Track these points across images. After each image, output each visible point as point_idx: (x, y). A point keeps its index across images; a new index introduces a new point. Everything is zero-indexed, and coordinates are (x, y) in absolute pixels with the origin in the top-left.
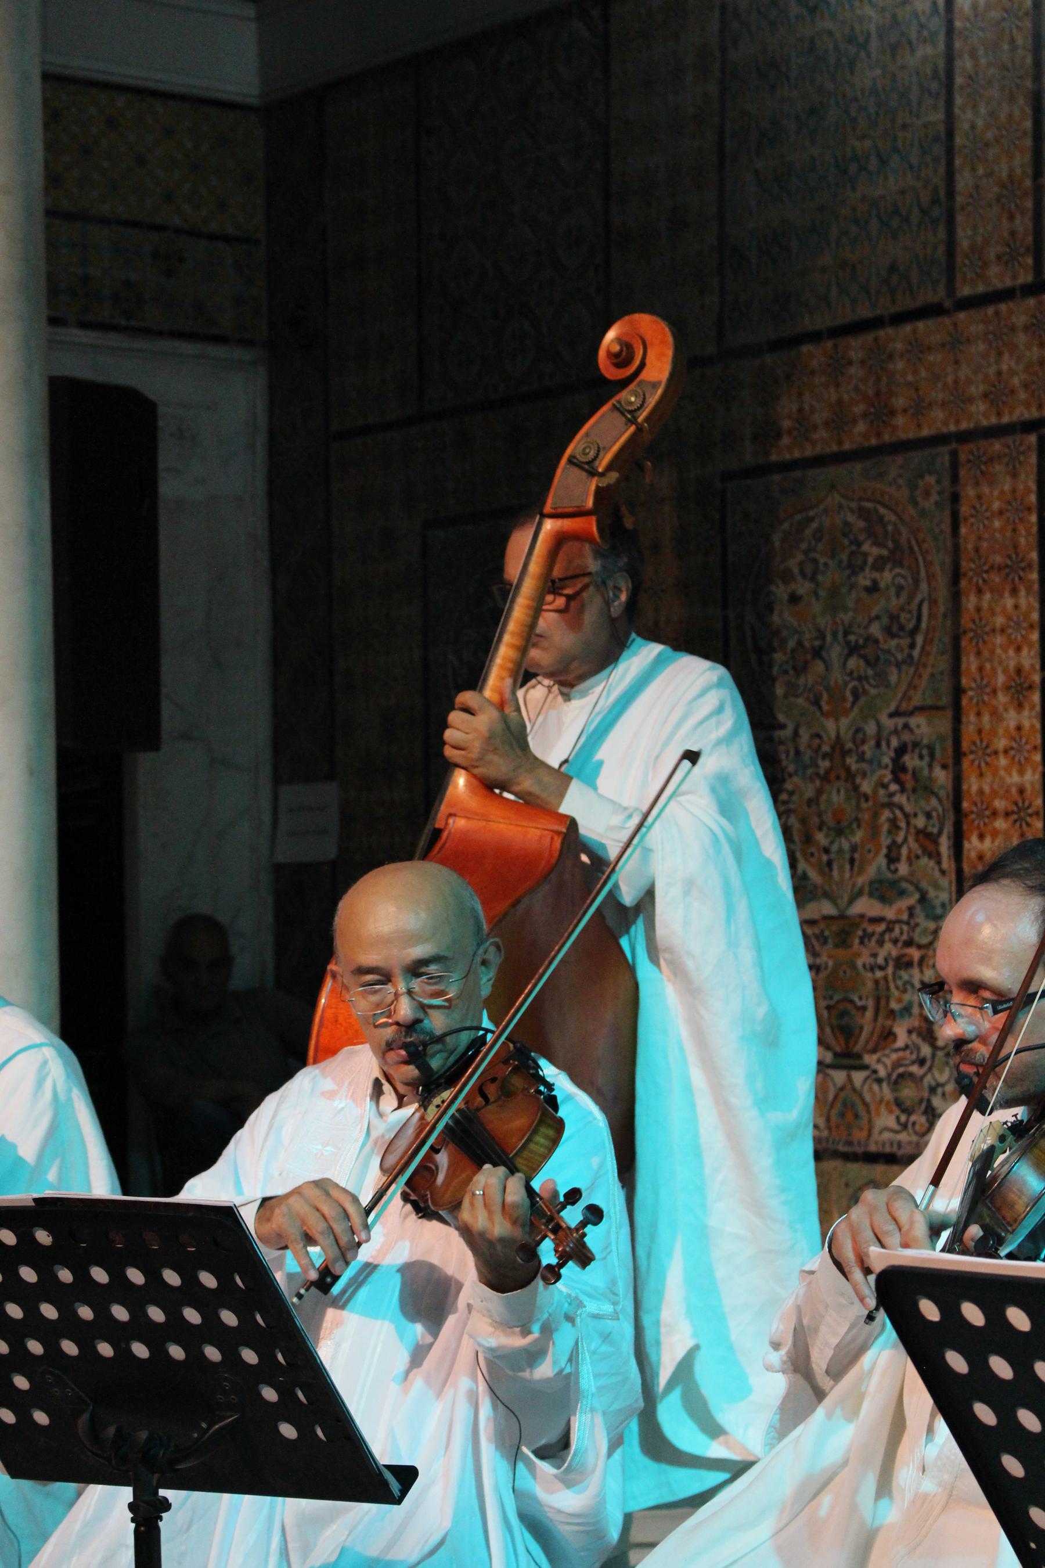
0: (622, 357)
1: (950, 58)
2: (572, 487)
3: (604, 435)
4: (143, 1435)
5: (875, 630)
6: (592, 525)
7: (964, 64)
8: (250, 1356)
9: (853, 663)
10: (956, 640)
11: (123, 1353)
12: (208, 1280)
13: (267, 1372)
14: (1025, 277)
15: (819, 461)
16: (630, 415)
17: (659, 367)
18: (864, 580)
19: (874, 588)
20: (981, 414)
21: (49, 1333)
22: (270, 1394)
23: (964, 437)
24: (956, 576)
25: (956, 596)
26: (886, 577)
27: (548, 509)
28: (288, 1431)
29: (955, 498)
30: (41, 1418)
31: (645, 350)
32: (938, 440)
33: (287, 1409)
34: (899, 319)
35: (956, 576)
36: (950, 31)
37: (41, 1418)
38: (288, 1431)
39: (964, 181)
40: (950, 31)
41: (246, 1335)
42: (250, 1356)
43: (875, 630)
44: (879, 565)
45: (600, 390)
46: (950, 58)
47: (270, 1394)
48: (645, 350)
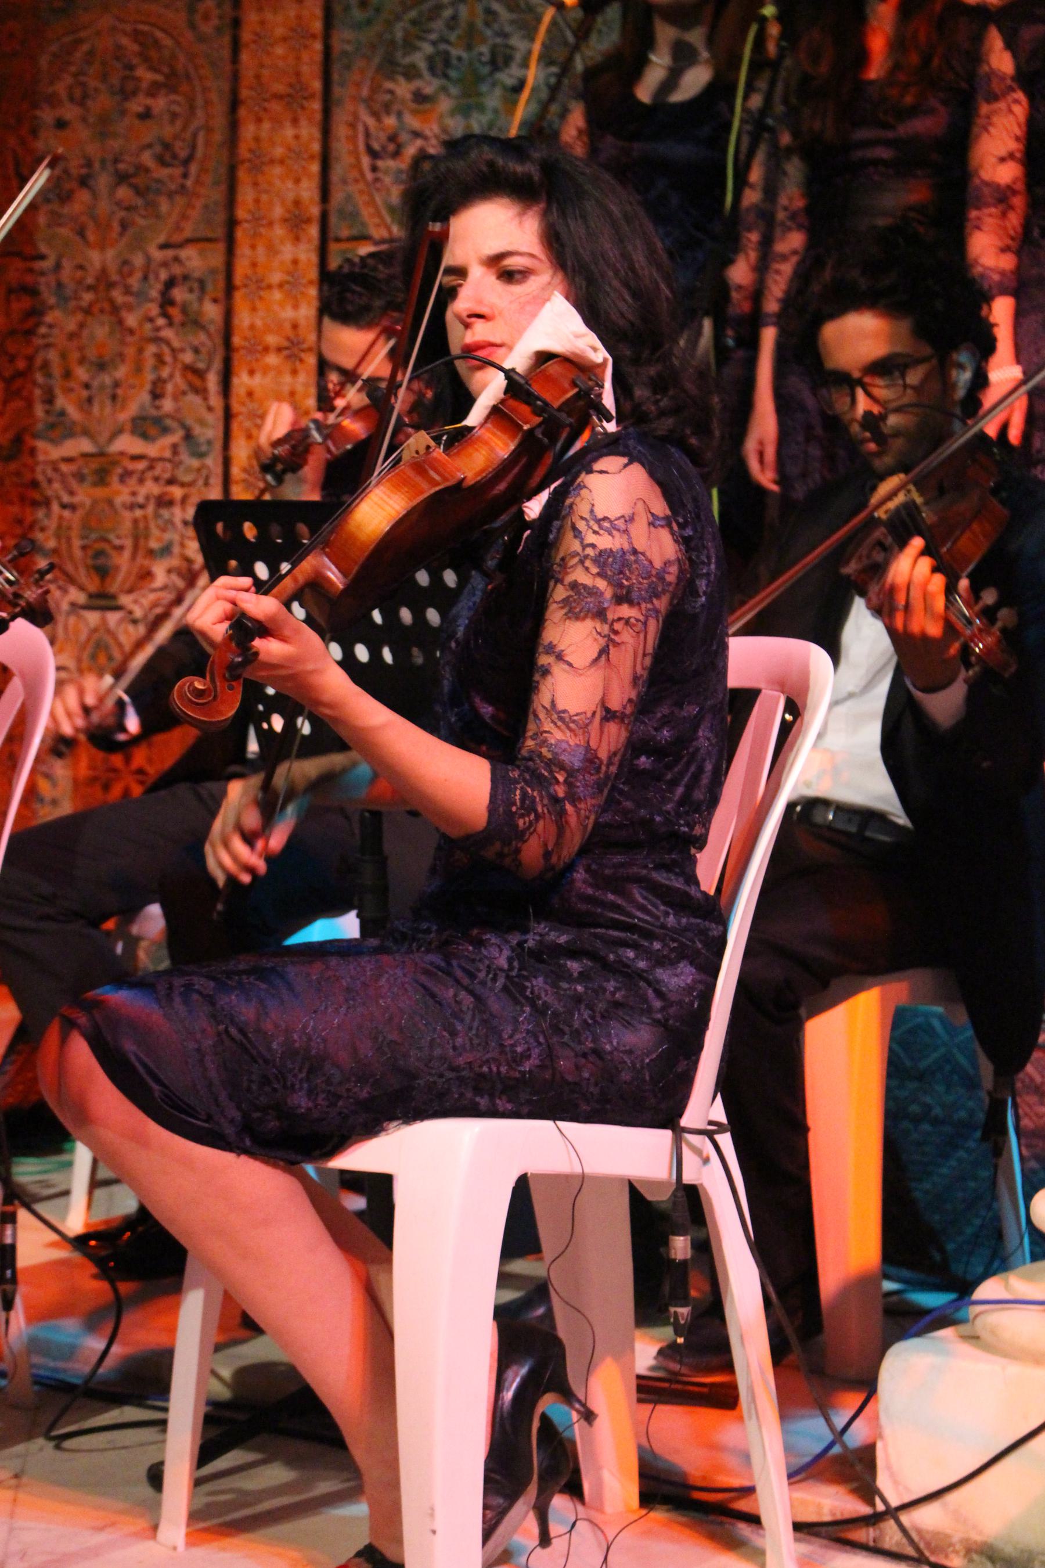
5: (147, 158)
9: (123, 192)
18: (136, 106)
19: (146, 115)
24: (234, 104)
25: (234, 126)
26: (160, 104)
29: (236, 23)
35: (234, 104)
43: (147, 158)
44: (154, 90)
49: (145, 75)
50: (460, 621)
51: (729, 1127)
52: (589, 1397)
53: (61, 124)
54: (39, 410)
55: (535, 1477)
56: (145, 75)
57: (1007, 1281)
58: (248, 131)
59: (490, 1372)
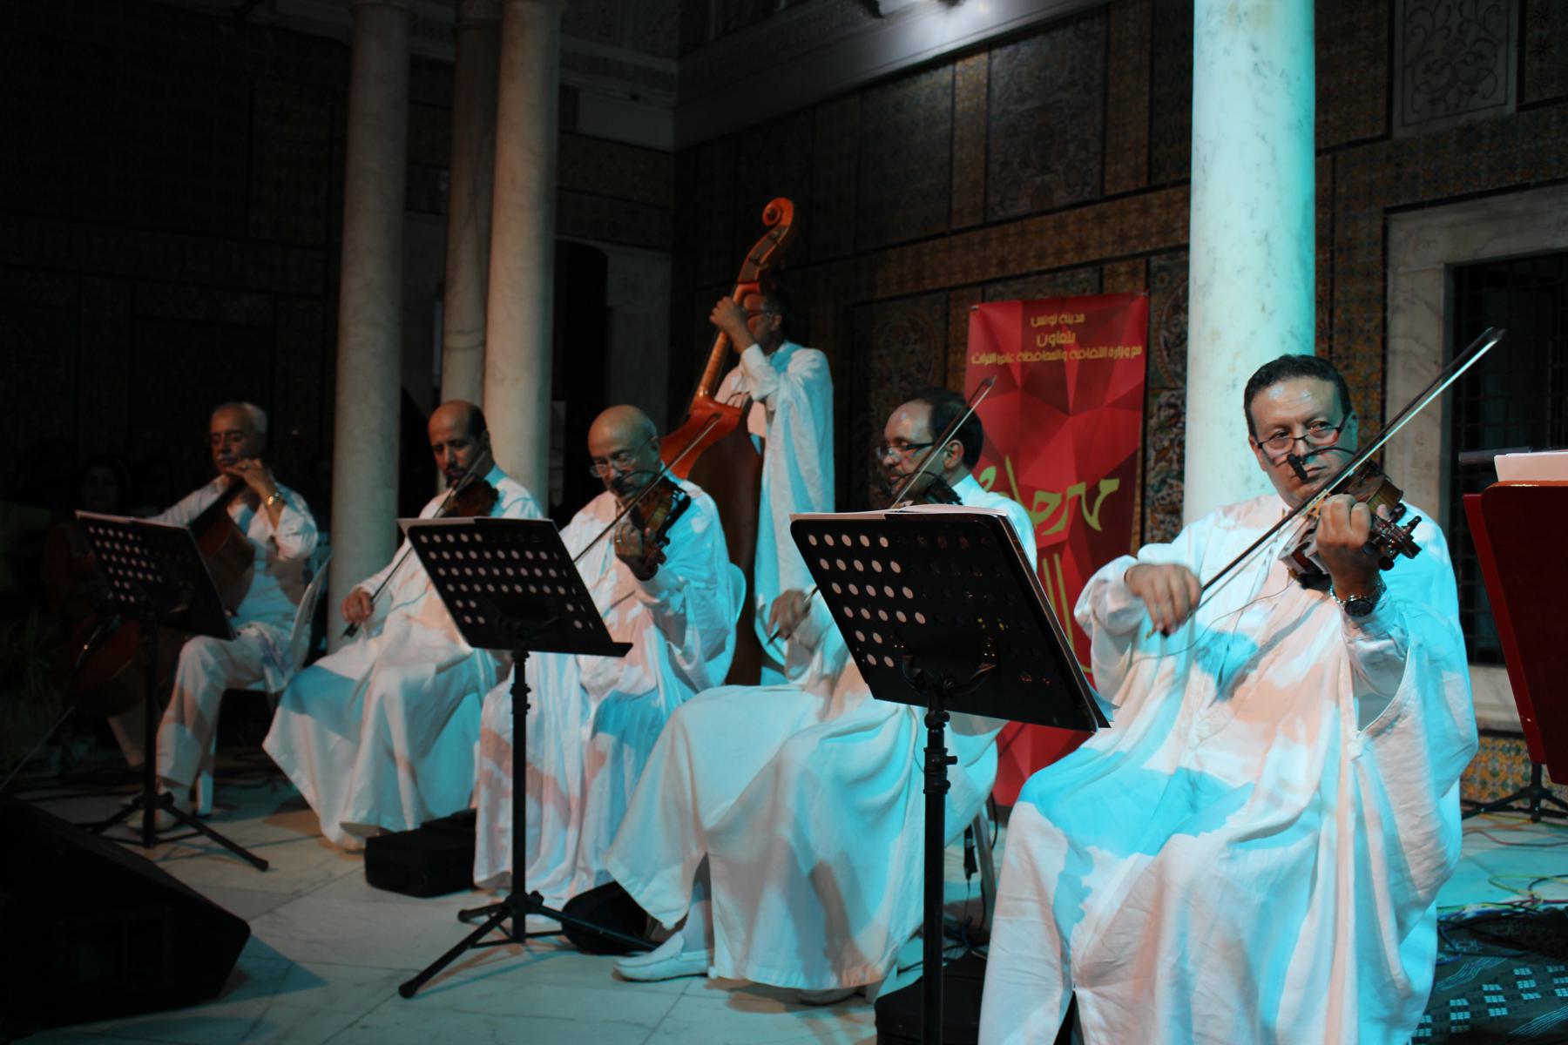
0: (772, 216)
1: (953, 130)
2: (750, 270)
3: (763, 250)
4: (518, 624)
5: (913, 370)
6: (757, 287)
7: (958, 133)
8: (562, 590)
9: (903, 383)
10: (946, 373)
11: (512, 590)
12: (544, 556)
13: (568, 598)
14: (980, 221)
15: (892, 299)
16: (774, 240)
17: (787, 220)
18: (909, 348)
19: (913, 352)
20: (959, 279)
21: (483, 581)
22: (570, 608)
23: (952, 288)
24: (946, 347)
25: (946, 356)
26: (918, 348)
27: (740, 278)
28: (578, 624)
29: (948, 314)
30: (481, 620)
31: (783, 213)
32: (942, 290)
33: (577, 615)
34: (928, 239)
35: (946, 347)
36: (953, 119)
37: (481, 620)
38: (578, 624)
39: (956, 181)
40: (953, 119)
41: (559, 581)
42: (562, 590)
43: (913, 370)
44: (916, 342)
45: (763, 230)
46: (953, 130)
47: (570, 608)
48: (783, 213)
49: (913, 336)
50: (1025, 359)
51: (1018, 724)
52: (664, 649)
53: (881, 357)
54: (871, 473)
55: (892, 511)
56: (913, 336)
57: (244, 978)
58: (952, 358)
59: (821, 451)
